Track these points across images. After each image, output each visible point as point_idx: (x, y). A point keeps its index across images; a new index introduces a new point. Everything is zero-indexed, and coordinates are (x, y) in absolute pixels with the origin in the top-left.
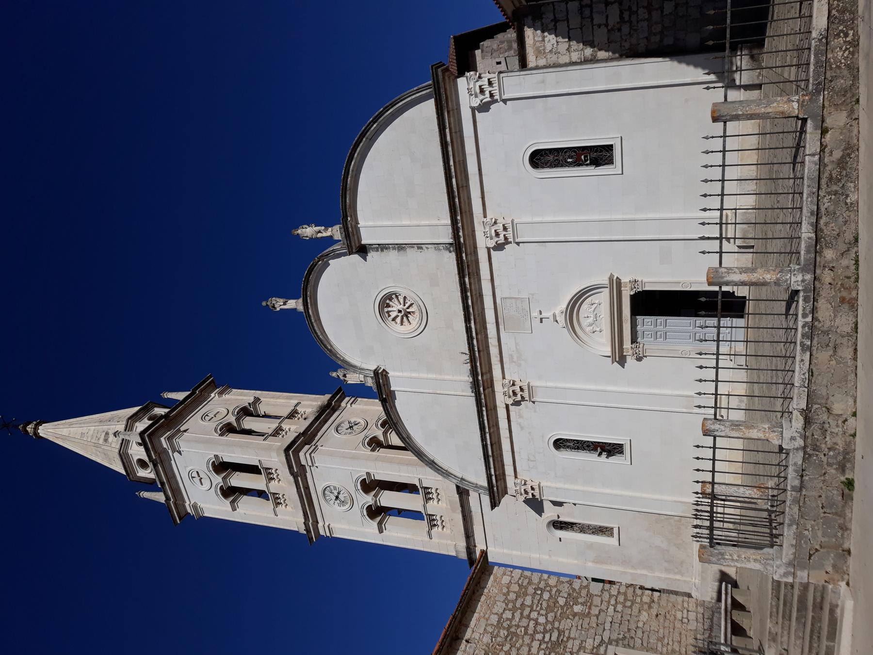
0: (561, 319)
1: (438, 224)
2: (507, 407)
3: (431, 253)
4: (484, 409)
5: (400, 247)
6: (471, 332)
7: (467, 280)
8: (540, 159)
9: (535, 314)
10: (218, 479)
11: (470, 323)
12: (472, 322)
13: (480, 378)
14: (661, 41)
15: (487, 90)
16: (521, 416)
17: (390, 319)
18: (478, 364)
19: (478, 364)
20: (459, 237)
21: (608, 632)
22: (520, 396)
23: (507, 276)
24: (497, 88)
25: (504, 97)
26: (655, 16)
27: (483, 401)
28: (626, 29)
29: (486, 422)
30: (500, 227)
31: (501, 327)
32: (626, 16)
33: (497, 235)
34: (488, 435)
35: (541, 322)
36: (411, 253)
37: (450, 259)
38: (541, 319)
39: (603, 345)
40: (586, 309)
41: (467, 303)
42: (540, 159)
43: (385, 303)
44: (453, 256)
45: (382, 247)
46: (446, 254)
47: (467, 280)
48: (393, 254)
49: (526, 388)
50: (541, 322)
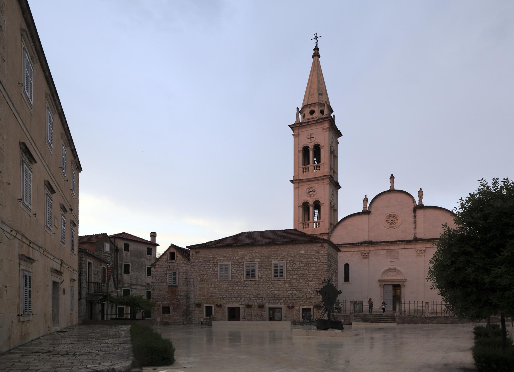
0: (392, 267)
3: (413, 231)
5: (415, 222)
10: (311, 146)
22: (366, 256)
37: (411, 238)
39: (386, 278)
40: (394, 273)
43: (394, 216)
44: (412, 239)
45: (415, 217)
46: (413, 236)
48: (413, 220)
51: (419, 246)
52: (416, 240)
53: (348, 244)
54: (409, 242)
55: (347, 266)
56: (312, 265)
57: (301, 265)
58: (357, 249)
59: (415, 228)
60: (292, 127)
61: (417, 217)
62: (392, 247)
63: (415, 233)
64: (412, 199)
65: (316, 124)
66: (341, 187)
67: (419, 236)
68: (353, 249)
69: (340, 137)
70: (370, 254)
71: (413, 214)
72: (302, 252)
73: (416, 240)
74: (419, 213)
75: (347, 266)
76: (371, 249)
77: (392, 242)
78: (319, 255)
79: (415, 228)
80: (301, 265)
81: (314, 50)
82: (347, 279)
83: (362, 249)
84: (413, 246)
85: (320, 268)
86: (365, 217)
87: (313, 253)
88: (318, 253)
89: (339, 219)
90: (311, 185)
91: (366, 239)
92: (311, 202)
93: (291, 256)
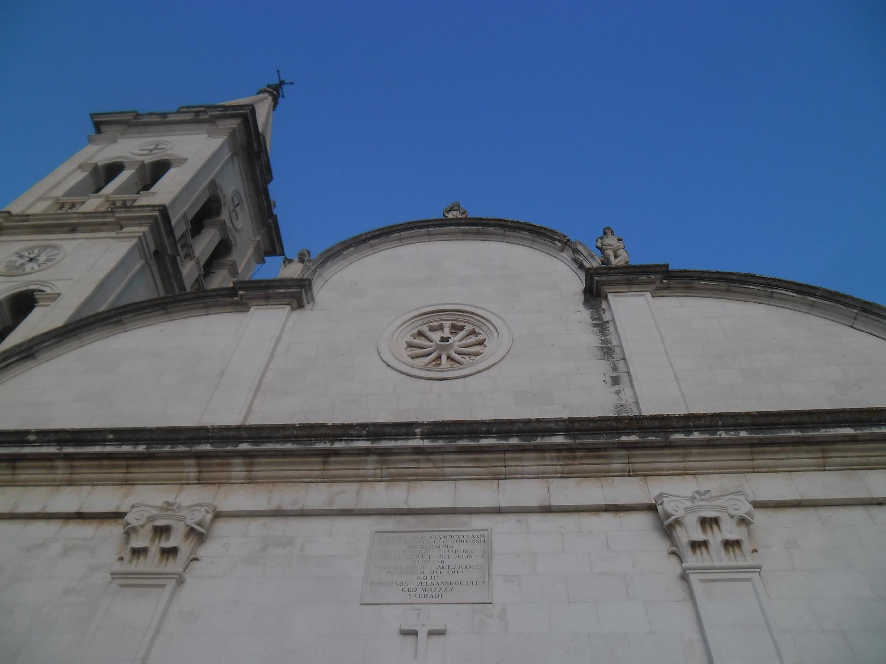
1: (656, 397)
2: (116, 516)
4: (141, 448)
6: (396, 437)
7: (559, 439)
9: (436, 617)
11: (424, 436)
12: (427, 443)
13: (244, 446)
15: (715, 538)
16: (66, 551)
17: (425, 329)
18: (289, 446)
19: (289, 446)
20: (687, 430)
21: (56, 438)
22: (162, 551)
24: (716, 563)
25: (694, 578)
27: (167, 448)
29: (97, 449)
30: (730, 531)
31: (390, 523)
33: (707, 523)
34: (52, 449)
35: (405, 633)
36: (602, 367)
38: (414, 633)
41: (488, 434)
47: (559, 439)
48: (592, 339)
49: (174, 566)
50: (405, 633)
53: (45, 436)
59: (616, 381)
64: (567, 255)
65: (193, 127)
70: (206, 551)
89: (16, 208)
90: (54, 243)
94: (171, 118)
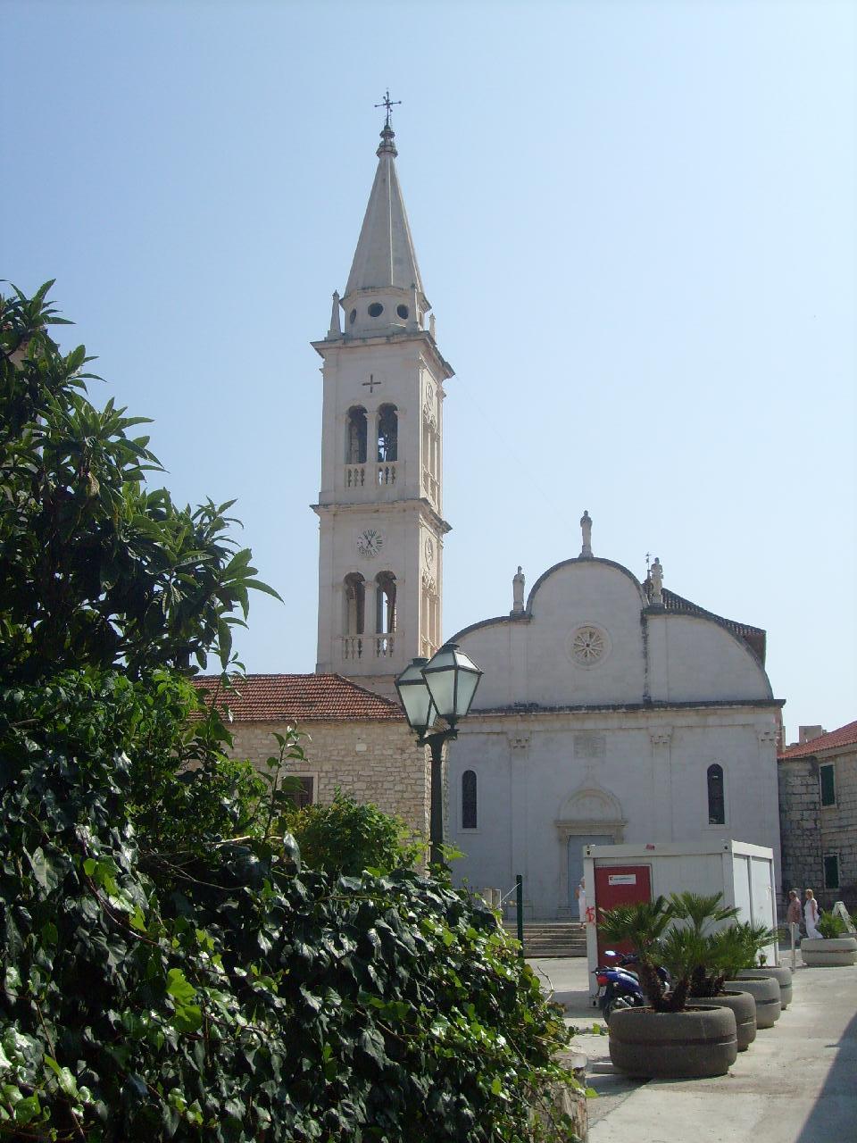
5: (646, 654)
8: (715, 774)
14: (790, 855)
23: (627, 742)
26: (805, 851)
28: (799, 832)
32: (808, 833)
37: (636, 696)
42: (715, 774)
45: (645, 638)
48: (639, 646)
51: (658, 722)
52: (649, 704)
54: (632, 708)
55: (469, 779)
56: (386, 785)
57: (357, 786)
58: (497, 727)
59: (646, 671)
60: (319, 347)
61: (650, 639)
62: (590, 724)
63: (646, 685)
66: (449, 528)
67: (657, 693)
68: (486, 728)
69: (448, 377)
71: (638, 629)
72: (361, 747)
73: (649, 704)
74: (656, 623)
75: (469, 779)
76: (537, 727)
77: (588, 708)
78: (405, 756)
79: (646, 671)
80: (357, 786)
81: (382, 135)
82: (469, 819)
83: (513, 725)
84: (642, 722)
85: (405, 795)
86: (518, 630)
87: (390, 752)
88: (403, 751)
91: (521, 695)
92: (370, 576)
93: (328, 759)
94: (383, 340)
